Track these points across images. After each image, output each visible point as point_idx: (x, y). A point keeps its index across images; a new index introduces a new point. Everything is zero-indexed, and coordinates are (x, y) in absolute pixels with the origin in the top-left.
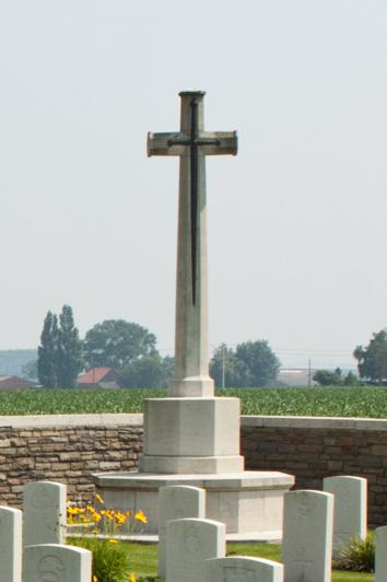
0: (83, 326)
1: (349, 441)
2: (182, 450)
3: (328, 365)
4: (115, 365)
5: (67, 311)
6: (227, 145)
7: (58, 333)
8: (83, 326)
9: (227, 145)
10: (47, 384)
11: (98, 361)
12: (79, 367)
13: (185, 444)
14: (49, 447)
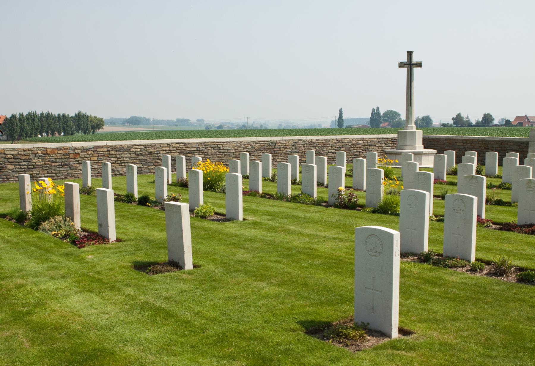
2: (407, 144)
3: (445, 122)
5: (378, 108)
6: (419, 65)
9: (419, 65)
10: (372, 127)
11: (386, 121)
12: (381, 122)
14: (373, 143)
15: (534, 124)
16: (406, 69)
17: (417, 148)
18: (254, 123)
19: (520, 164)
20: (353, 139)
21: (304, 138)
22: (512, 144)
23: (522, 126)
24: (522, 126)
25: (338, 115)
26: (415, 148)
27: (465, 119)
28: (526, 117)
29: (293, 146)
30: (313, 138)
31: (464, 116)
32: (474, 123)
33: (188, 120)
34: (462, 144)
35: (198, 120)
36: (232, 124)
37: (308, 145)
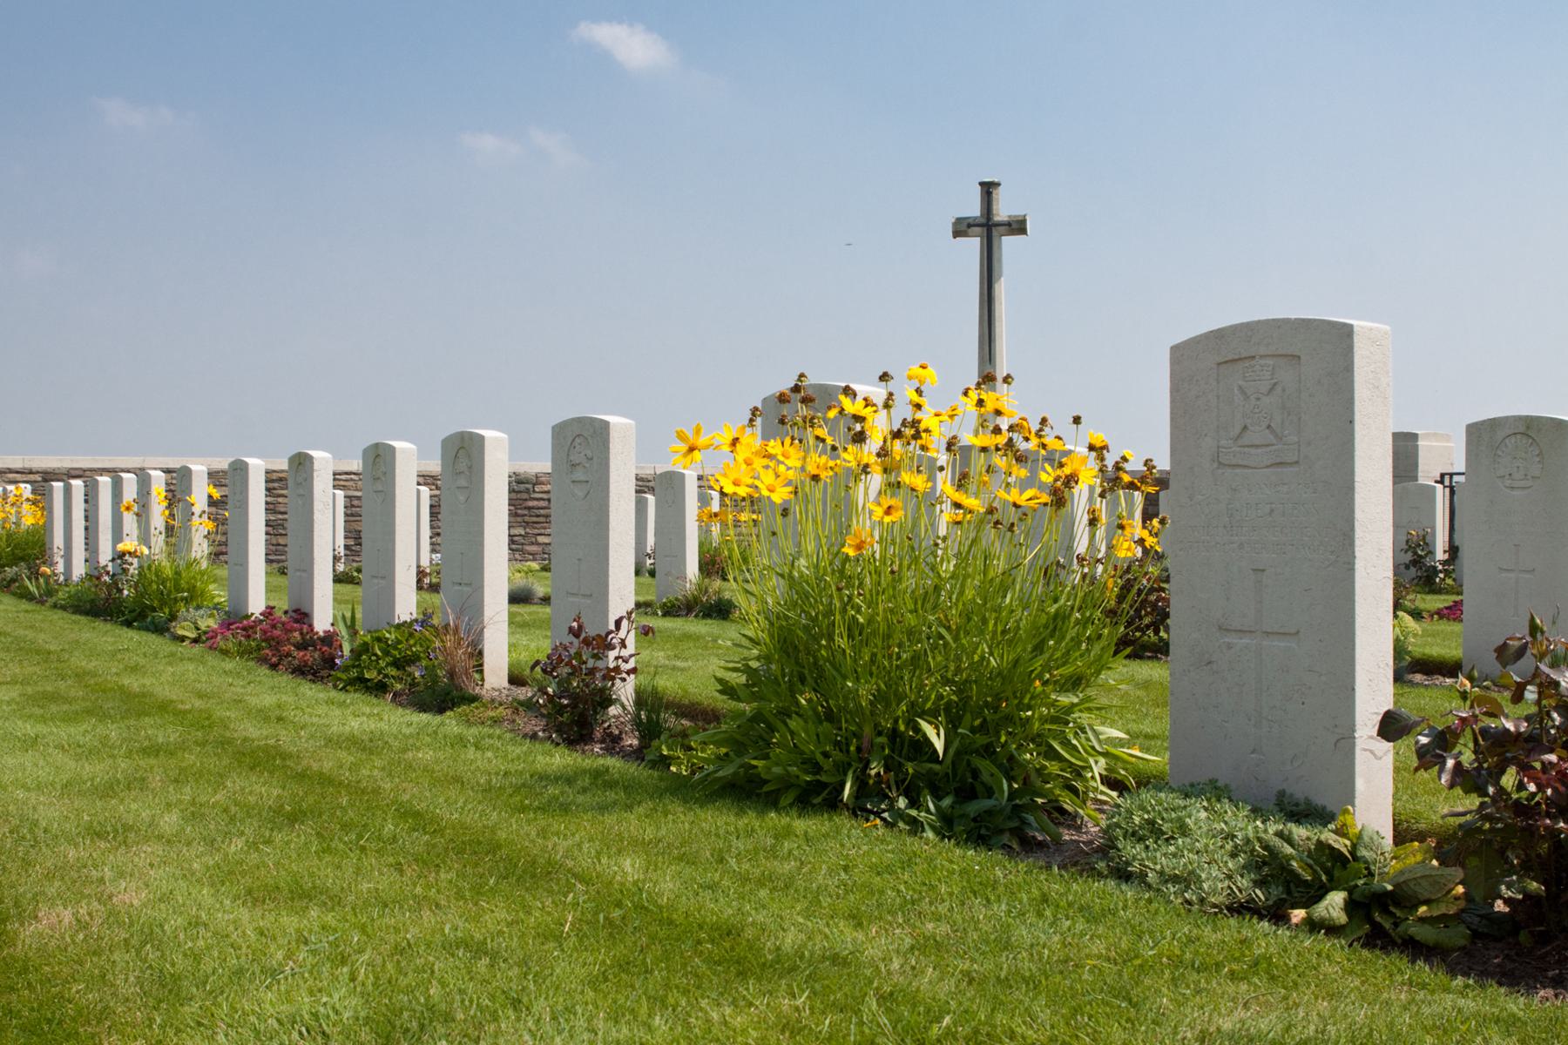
6: (1018, 227)
9: (1018, 227)
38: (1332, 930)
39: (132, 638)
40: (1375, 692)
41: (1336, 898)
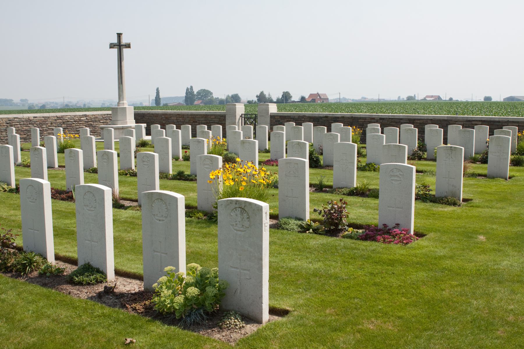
0: (195, 91)
1: (167, 116)
2: (119, 119)
3: (250, 99)
4: (203, 100)
5: (192, 87)
6: (128, 46)
7: (189, 93)
8: (195, 91)
9: (128, 46)
10: (187, 104)
11: (199, 99)
12: (195, 100)
13: (119, 117)
14: (97, 119)
15: (324, 100)
16: (117, 49)
17: (128, 123)
18: (78, 102)
19: (192, 137)
20: (75, 116)
21: (20, 116)
22: (214, 117)
23: (315, 102)
24: (315, 102)
25: (156, 94)
26: (126, 123)
27: (267, 96)
28: (318, 94)
29: (8, 124)
30: (31, 116)
31: (266, 93)
32: (275, 100)
33: (12, 100)
34: (175, 118)
35: (22, 100)
36: (56, 103)
37: (25, 123)
38: (310, 233)
39: (134, 177)
40: (113, 140)
41: (311, 230)
